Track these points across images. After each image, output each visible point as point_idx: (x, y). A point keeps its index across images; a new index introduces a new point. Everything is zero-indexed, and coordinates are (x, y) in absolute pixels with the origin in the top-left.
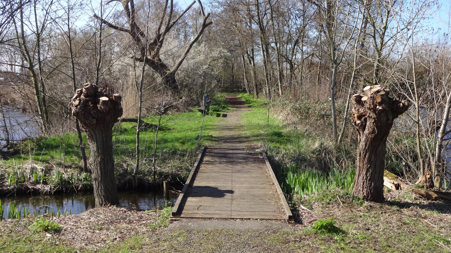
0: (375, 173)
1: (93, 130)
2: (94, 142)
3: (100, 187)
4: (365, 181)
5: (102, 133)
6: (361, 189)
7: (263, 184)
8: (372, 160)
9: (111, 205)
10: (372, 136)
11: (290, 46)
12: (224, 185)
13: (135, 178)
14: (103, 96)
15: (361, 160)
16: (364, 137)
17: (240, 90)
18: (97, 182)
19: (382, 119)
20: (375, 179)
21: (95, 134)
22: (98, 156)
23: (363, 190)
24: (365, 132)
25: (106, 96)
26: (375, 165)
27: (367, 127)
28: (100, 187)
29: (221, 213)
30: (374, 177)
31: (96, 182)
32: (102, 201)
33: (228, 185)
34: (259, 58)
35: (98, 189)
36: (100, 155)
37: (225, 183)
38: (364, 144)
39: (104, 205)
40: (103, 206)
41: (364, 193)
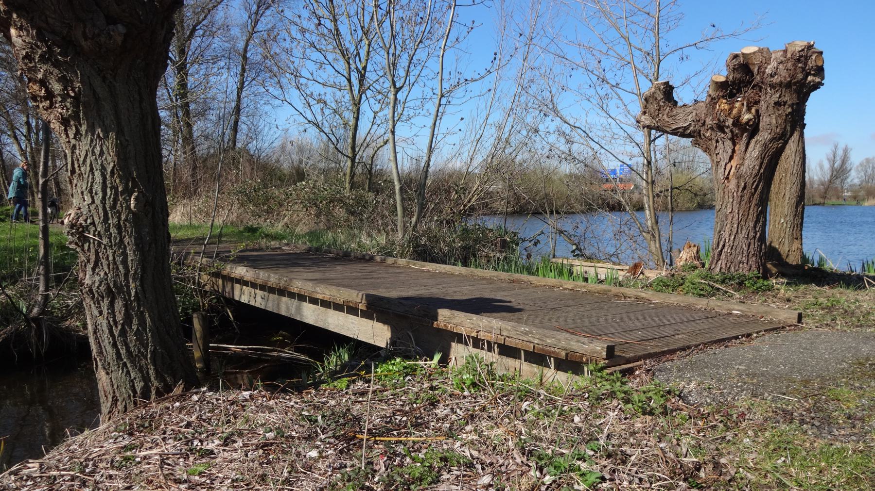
1: (104, 79)
2: (106, 133)
3: (135, 321)
9: (187, 389)
15: (746, 198)
18: (119, 305)
22: (128, 192)
28: (135, 321)
31: (112, 305)
32: (146, 379)
35: (123, 333)
36: (135, 185)
39: (159, 394)
40: (153, 396)
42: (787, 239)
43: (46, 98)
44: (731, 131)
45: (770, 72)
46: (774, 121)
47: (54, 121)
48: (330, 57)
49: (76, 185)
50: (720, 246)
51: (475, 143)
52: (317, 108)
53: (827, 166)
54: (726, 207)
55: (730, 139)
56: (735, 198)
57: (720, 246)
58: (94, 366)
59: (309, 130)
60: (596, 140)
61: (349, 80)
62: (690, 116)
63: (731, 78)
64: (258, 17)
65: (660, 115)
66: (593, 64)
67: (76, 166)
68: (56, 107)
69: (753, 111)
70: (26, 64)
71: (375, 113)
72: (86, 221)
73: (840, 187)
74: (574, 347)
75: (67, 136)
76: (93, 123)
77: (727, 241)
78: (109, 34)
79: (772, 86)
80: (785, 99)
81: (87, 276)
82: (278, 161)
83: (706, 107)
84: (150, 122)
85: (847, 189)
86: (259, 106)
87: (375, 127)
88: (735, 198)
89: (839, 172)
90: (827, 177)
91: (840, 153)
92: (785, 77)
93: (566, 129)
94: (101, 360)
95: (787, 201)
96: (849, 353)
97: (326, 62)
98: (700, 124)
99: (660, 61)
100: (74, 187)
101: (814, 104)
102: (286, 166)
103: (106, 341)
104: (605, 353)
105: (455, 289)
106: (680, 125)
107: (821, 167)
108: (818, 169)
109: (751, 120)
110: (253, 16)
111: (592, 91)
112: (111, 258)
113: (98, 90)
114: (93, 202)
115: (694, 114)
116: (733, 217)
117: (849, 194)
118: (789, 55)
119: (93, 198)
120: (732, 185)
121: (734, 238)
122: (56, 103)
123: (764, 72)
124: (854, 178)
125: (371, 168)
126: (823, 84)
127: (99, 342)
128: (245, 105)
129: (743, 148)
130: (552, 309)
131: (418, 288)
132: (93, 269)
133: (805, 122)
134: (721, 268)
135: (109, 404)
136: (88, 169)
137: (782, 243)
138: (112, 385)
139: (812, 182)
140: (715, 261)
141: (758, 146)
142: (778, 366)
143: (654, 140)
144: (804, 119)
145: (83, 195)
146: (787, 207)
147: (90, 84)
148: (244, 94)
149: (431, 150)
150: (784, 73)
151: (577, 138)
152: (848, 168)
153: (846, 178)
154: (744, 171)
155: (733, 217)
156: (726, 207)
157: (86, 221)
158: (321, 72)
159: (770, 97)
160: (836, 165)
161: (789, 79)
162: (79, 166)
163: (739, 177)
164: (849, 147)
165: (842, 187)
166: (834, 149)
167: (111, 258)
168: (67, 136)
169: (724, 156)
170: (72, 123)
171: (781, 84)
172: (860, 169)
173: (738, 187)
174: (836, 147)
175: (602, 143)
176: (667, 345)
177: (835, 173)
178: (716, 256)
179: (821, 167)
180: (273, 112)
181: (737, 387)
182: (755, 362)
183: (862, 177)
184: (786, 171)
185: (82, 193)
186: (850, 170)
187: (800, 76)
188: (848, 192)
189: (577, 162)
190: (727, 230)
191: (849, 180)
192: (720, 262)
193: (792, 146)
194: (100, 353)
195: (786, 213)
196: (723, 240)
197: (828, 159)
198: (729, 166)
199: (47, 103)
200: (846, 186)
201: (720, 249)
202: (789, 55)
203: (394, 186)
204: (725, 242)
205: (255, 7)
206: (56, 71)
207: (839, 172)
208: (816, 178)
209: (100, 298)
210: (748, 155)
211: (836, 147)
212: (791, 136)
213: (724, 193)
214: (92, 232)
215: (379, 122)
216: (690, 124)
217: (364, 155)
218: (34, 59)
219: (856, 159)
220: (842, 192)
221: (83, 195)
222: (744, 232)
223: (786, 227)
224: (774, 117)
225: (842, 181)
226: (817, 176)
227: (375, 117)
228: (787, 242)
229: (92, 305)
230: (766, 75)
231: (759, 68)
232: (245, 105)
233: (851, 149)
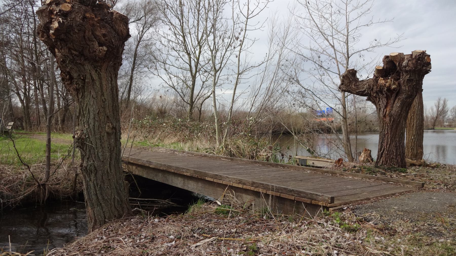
1: (96, 71)
4: (398, 148)
21: (100, 78)
41: (398, 160)
42: (415, 147)
43: (69, 80)
44: (386, 94)
45: (405, 65)
46: (407, 89)
47: (72, 90)
48: (181, 54)
49: (81, 120)
50: (382, 150)
51: (254, 97)
52: (174, 79)
53: (435, 109)
54: (384, 131)
55: (385, 97)
56: (389, 127)
57: (382, 150)
58: (86, 205)
59: (170, 91)
60: (318, 96)
61: (190, 66)
62: (366, 86)
63: (385, 67)
64: (143, 34)
65: (351, 85)
66: (316, 58)
67: (81, 111)
68: (73, 84)
69: (397, 83)
70: (62, 65)
71: (203, 82)
72: (85, 136)
73: (442, 120)
74: (315, 198)
75: (78, 96)
76: (90, 91)
77: (109, 170)
78: (100, 51)
79: (406, 72)
80: (412, 78)
81: (85, 162)
82: (151, 106)
83: (373, 81)
84: (115, 90)
85: (446, 121)
86: (142, 78)
87: (203, 89)
88: (389, 127)
89: (442, 112)
90: (435, 115)
91: (442, 102)
92: (412, 67)
93: (303, 91)
94: (89, 202)
95: (415, 128)
96: (447, 201)
97: (179, 57)
98: (370, 90)
99: (349, 57)
100: (80, 121)
101: (427, 80)
102: (155, 108)
103: (92, 193)
104: (330, 201)
105: (251, 171)
106: (361, 90)
107: (432, 110)
108: (431, 110)
109: (396, 88)
110: (140, 33)
111: (316, 72)
112: (96, 154)
113: (94, 76)
114: (89, 127)
115: (367, 85)
116: (388, 136)
117: (447, 124)
118: (414, 57)
119: (89, 125)
120: (387, 119)
121: (389, 146)
122: (74, 82)
123: (402, 65)
124: (449, 115)
125: (201, 109)
126: (431, 71)
127: (89, 194)
128: (135, 78)
129: (392, 102)
130: (300, 181)
131: (232, 170)
132: (88, 158)
133: (423, 88)
134: (383, 161)
135: (92, 224)
136: (87, 112)
137: (413, 149)
138: (94, 215)
139: (427, 117)
140: (380, 158)
141: (400, 101)
142: (413, 207)
143: (347, 96)
144: (422, 87)
145: (84, 124)
146: (415, 131)
147: (90, 73)
148: (134, 72)
149: (233, 101)
150: (411, 65)
151: (308, 96)
152: (446, 111)
153: (445, 115)
154: (393, 113)
155: (388, 136)
156: (384, 131)
157: (85, 136)
158: (177, 61)
159: (405, 77)
160: (440, 109)
161: (414, 69)
162: (83, 111)
163: (391, 116)
164: (447, 99)
165: (443, 121)
166: (438, 100)
167: (96, 154)
168: (78, 96)
169: (382, 106)
170: (81, 91)
171: (410, 70)
172: (452, 111)
173: (390, 120)
174: (439, 100)
175: (321, 98)
176: (359, 197)
177: (439, 113)
178: (380, 155)
179: (432, 110)
180: (149, 81)
181: (394, 216)
182: (402, 206)
183: (454, 115)
184: (414, 112)
185: (84, 123)
186: (447, 111)
187: (419, 67)
188: (446, 123)
189: (308, 107)
190: (385, 142)
191: (447, 117)
192: (382, 158)
193: (416, 100)
194: (89, 199)
195: (414, 134)
196: (383, 147)
197: (436, 106)
198: (385, 110)
199: (69, 82)
200: (445, 120)
201: (382, 152)
202: (414, 57)
203: (215, 119)
204: (384, 148)
205: (141, 29)
206: (75, 68)
207: (442, 112)
208: (429, 115)
209: (90, 173)
210: (395, 105)
211: (439, 100)
212: (416, 96)
213: (383, 124)
214: (88, 142)
215: (205, 87)
216: (365, 90)
217: (198, 103)
218: (66, 62)
219: (450, 106)
220: (443, 123)
221: (84, 124)
222: (394, 143)
223: (415, 141)
224: (407, 87)
225: (444, 117)
226: (430, 114)
227: (203, 84)
228: (415, 148)
229: (86, 176)
230: (402, 66)
231: (399, 63)
232: (135, 78)
233: (448, 101)
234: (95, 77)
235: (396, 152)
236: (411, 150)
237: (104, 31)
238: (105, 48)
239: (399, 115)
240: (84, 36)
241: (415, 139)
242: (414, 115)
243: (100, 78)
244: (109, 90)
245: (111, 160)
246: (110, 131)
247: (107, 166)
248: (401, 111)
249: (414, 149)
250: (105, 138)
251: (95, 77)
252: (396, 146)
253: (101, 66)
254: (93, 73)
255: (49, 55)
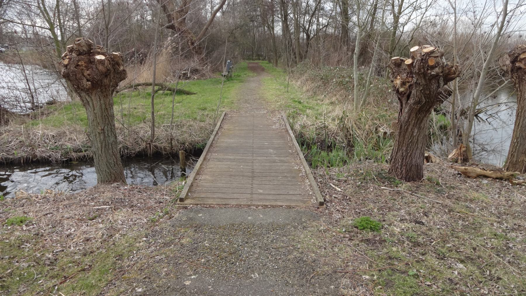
0: (417, 149)
1: (89, 96)
4: (405, 158)
5: (100, 99)
6: (399, 167)
7: (286, 157)
8: (415, 134)
10: (417, 107)
11: (307, 17)
12: (244, 157)
13: (150, 146)
14: (99, 53)
16: (408, 108)
17: (261, 58)
19: (432, 87)
20: (416, 156)
21: (92, 100)
23: (401, 169)
24: (409, 102)
25: (103, 54)
26: (418, 140)
27: (412, 96)
29: (238, 197)
30: (415, 154)
33: (248, 158)
34: (278, 29)
37: (245, 155)
38: (407, 115)
41: (402, 171)
195: (518, 136)
223: (517, 145)
234: (89, 99)
235: (402, 161)
236: (511, 156)
237: (88, 72)
238: (90, 83)
239: (407, 122)
240: (76, 78)
241: (517, 143)
242: (521, 112)
243: (92, 100)
244: (98, 107)
245: (102, 148)
246: (100, 131)
247: (100, 152)
248: (409, 118)
249: (514, 156)
250: (98, 135)
251: (89, 99)
252: (402, 156)
253: (91, 93)
254: (87, 97)
255: (271, 19)
